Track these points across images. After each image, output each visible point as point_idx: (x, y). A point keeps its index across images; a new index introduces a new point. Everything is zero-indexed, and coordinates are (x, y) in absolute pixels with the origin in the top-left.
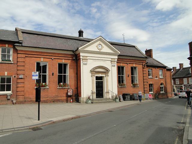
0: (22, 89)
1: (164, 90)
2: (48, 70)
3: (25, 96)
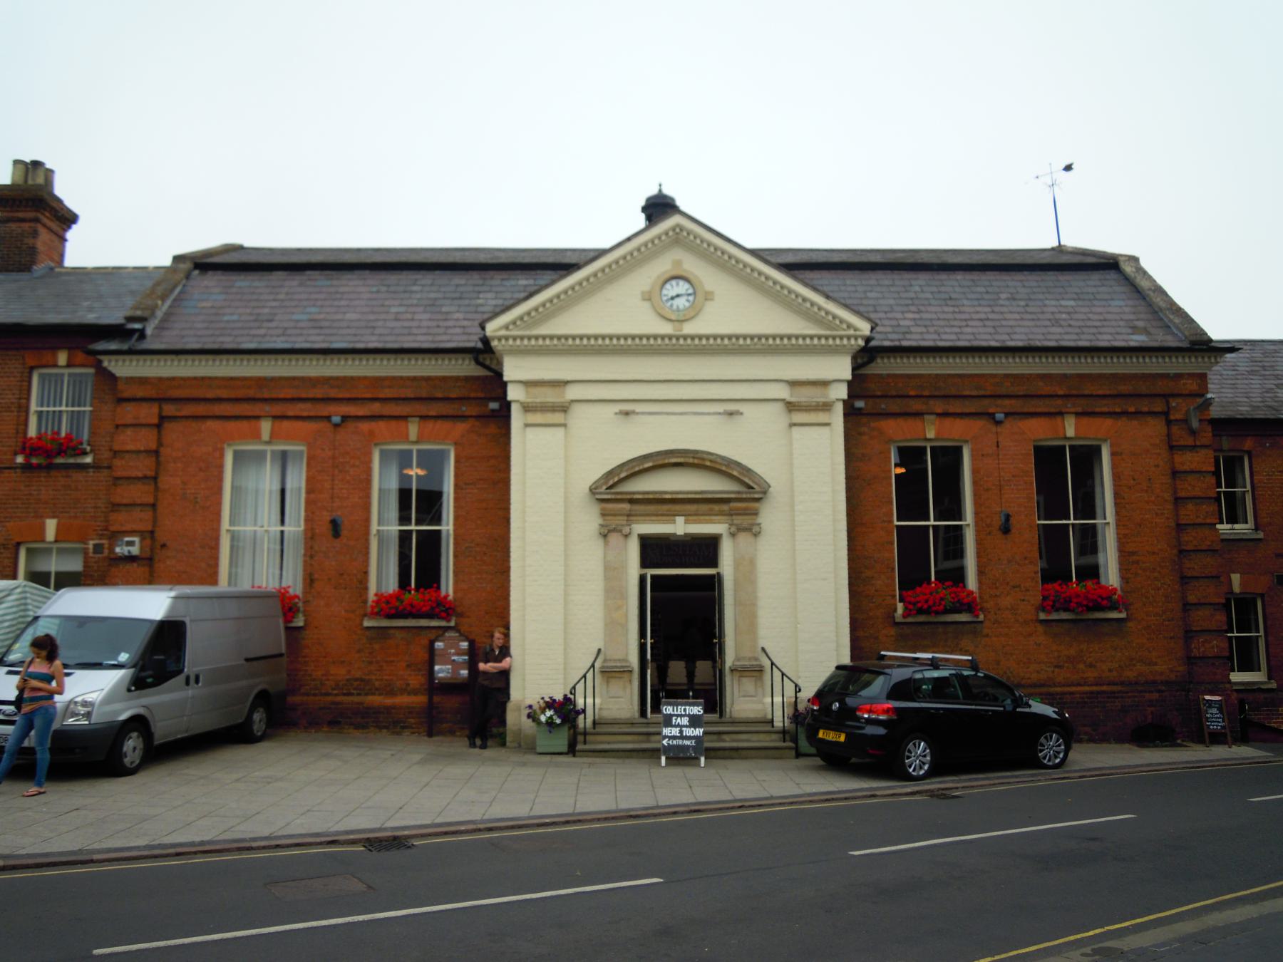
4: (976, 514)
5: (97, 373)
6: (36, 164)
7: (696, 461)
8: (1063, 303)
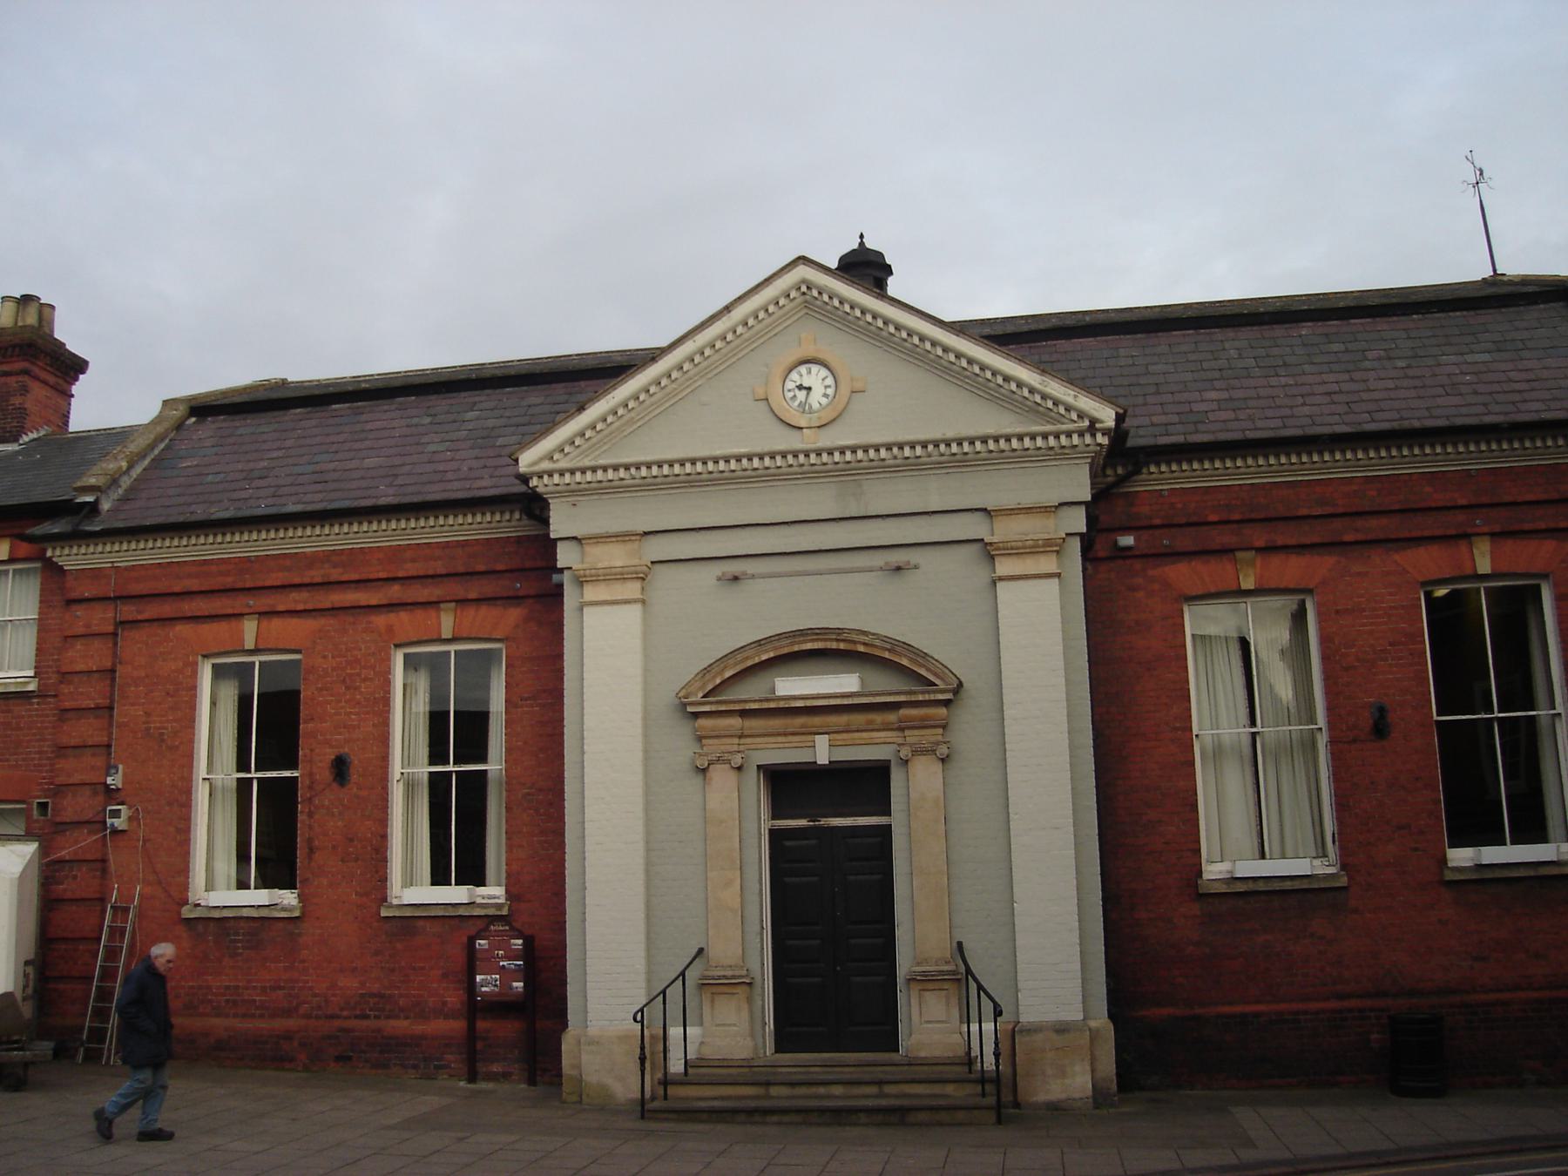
4: (1330, 709)
5: (44, 569)
6: (27, 299)
7: (842, 646)
8: (1469, 358)
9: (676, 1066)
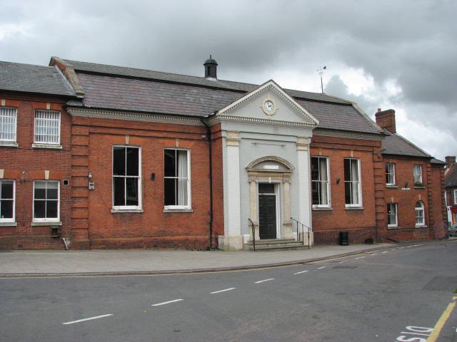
0: (83, 213)
1: (424, 220)
2: (142, 167)
3: (90, 230)
9: (426, 226)
